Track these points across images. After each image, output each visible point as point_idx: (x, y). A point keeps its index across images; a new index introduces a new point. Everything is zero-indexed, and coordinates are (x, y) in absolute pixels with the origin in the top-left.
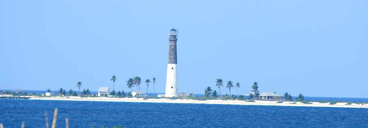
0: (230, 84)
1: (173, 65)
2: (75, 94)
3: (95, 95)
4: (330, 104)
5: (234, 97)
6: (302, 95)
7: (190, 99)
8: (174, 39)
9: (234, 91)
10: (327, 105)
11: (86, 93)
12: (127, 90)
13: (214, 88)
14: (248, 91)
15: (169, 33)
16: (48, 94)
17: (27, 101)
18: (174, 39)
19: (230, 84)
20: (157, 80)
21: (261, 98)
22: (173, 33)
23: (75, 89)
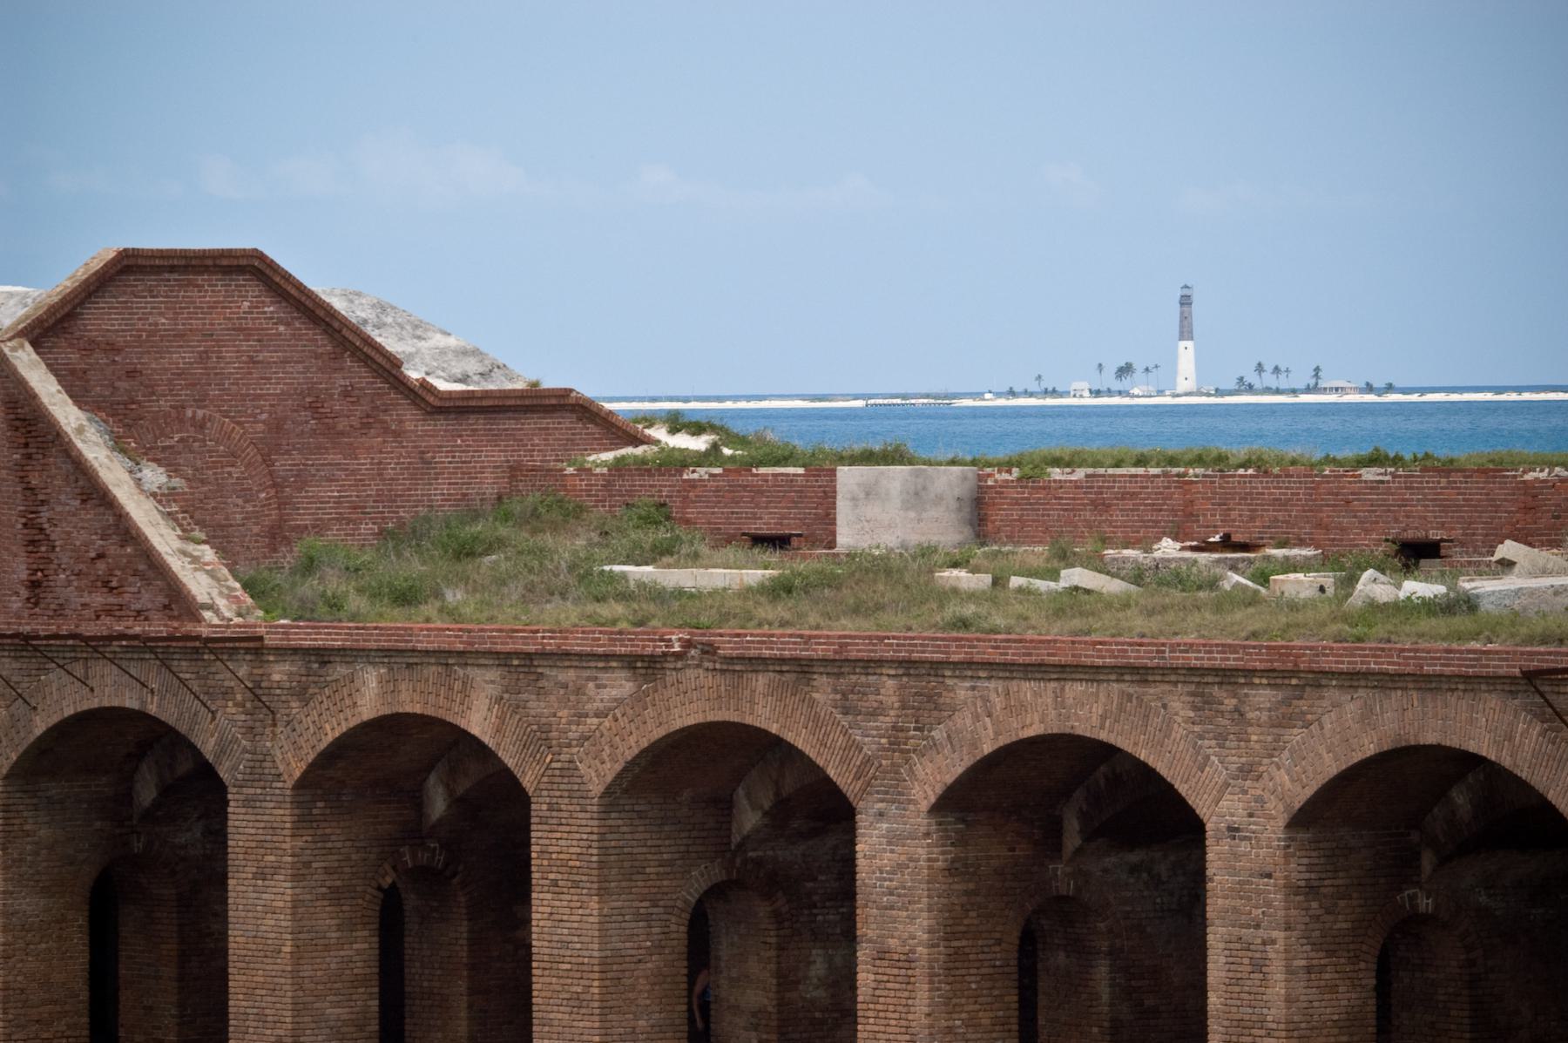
0: (1277, 370)
1: (1189, 344)
2: (1031, 395)
3: (1061, 395)
4: (160, 497)
5: (1278, 392)
6: (399, 555)
7: (1329, 460)
8: (1186, 301)
9: (1283, 383)
10: (1414, 398)
11: (1054, 393)
12: (1116, 385)
13: (1252, 378)
14: (1302, 378)
15: (1179, 293)
16: (988, 396)
17: (601, 409)
18: (1186, 301)
19: (1277, 370)
20: (1160, 369)
21: (1324, 391)
22: (1186, 292)
23: (1034, 387)
